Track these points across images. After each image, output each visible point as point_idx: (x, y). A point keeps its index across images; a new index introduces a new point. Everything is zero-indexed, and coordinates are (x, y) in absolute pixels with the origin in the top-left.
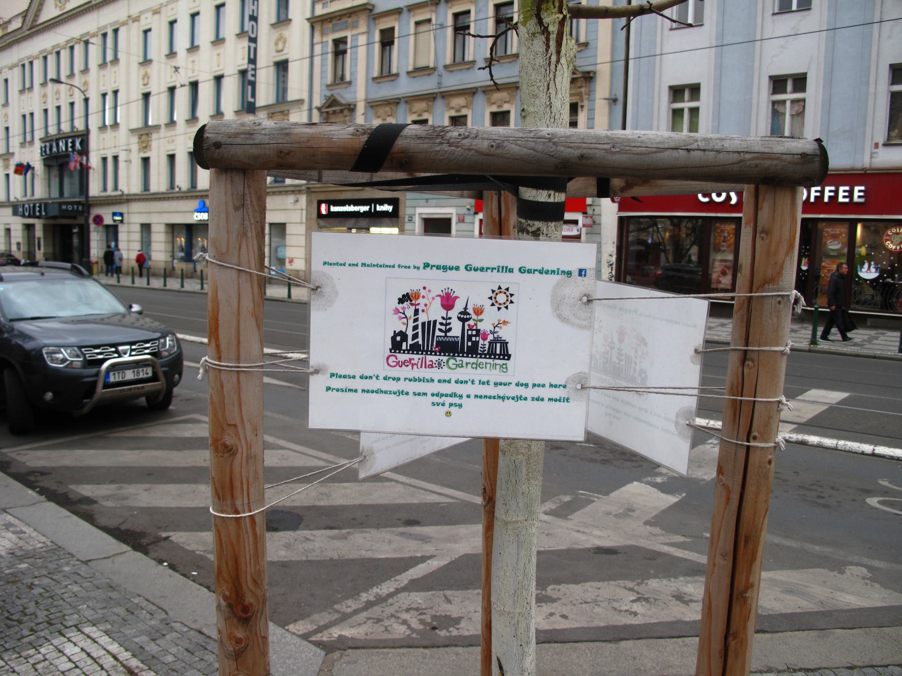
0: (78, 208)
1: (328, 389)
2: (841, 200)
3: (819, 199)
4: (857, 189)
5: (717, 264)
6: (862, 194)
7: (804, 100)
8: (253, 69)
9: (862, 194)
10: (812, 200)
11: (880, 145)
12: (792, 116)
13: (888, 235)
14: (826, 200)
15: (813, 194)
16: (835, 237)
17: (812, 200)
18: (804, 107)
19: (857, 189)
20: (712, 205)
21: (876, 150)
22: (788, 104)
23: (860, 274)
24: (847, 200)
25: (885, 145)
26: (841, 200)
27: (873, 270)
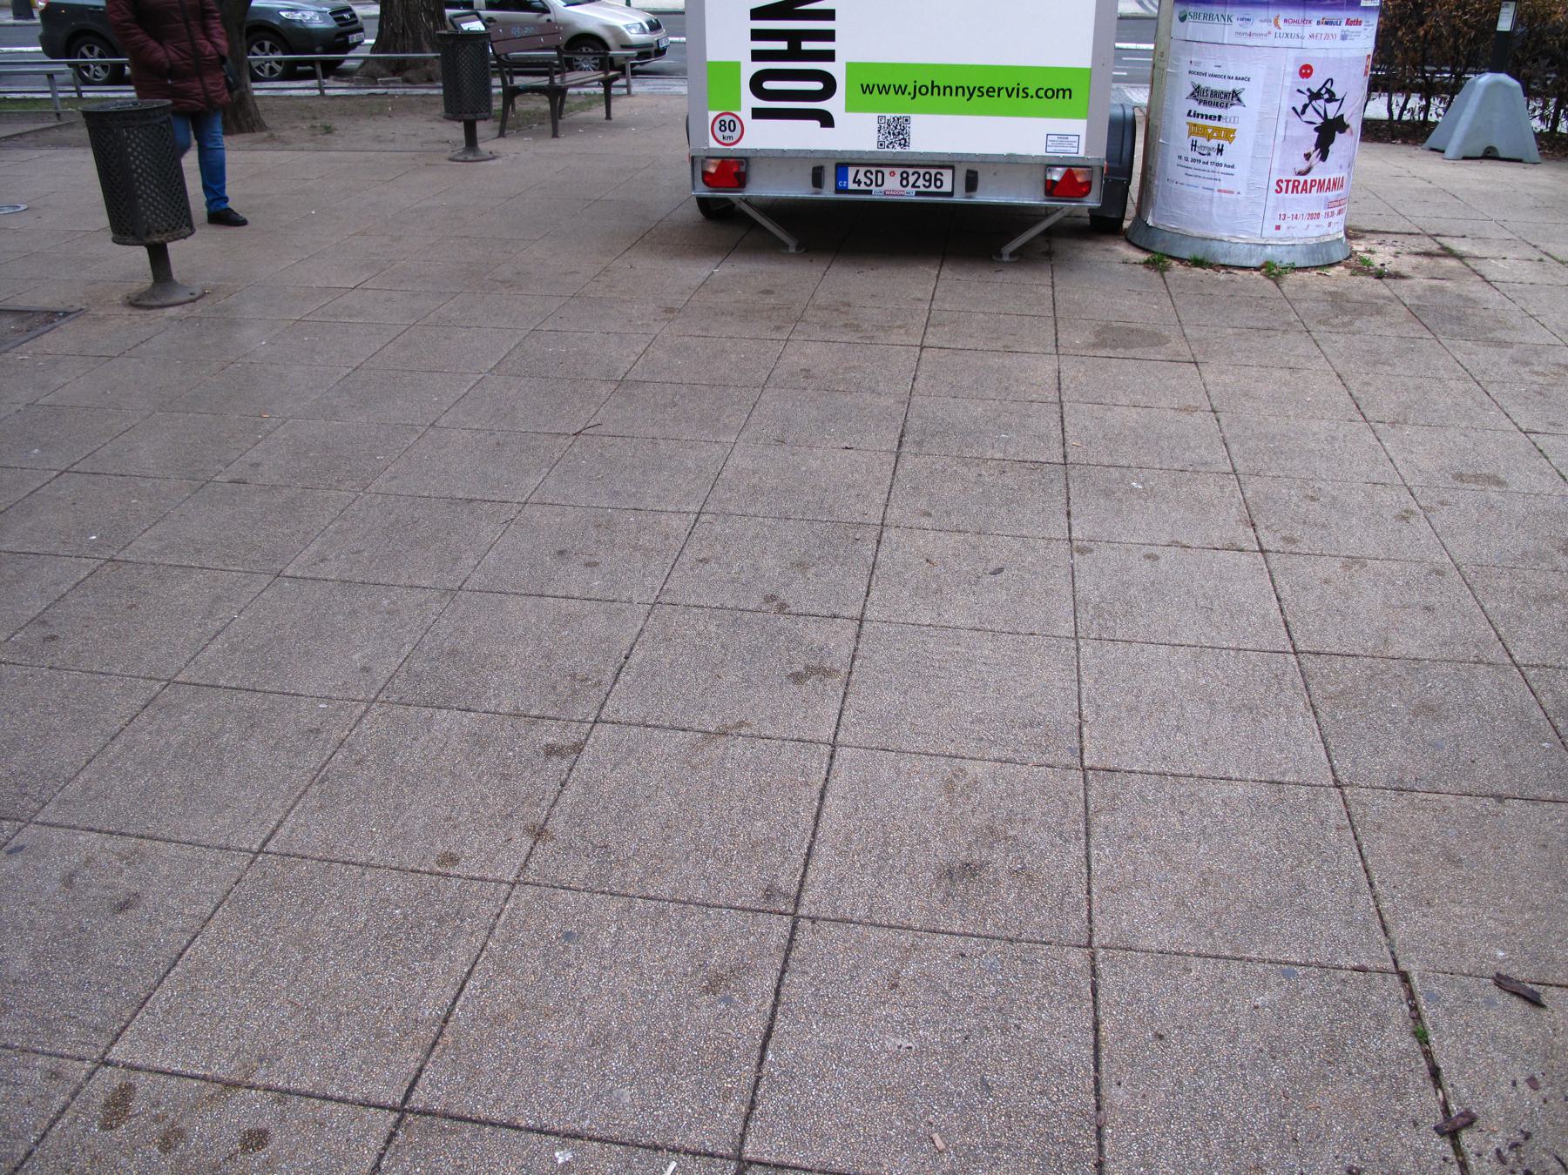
1: (1233, 167)
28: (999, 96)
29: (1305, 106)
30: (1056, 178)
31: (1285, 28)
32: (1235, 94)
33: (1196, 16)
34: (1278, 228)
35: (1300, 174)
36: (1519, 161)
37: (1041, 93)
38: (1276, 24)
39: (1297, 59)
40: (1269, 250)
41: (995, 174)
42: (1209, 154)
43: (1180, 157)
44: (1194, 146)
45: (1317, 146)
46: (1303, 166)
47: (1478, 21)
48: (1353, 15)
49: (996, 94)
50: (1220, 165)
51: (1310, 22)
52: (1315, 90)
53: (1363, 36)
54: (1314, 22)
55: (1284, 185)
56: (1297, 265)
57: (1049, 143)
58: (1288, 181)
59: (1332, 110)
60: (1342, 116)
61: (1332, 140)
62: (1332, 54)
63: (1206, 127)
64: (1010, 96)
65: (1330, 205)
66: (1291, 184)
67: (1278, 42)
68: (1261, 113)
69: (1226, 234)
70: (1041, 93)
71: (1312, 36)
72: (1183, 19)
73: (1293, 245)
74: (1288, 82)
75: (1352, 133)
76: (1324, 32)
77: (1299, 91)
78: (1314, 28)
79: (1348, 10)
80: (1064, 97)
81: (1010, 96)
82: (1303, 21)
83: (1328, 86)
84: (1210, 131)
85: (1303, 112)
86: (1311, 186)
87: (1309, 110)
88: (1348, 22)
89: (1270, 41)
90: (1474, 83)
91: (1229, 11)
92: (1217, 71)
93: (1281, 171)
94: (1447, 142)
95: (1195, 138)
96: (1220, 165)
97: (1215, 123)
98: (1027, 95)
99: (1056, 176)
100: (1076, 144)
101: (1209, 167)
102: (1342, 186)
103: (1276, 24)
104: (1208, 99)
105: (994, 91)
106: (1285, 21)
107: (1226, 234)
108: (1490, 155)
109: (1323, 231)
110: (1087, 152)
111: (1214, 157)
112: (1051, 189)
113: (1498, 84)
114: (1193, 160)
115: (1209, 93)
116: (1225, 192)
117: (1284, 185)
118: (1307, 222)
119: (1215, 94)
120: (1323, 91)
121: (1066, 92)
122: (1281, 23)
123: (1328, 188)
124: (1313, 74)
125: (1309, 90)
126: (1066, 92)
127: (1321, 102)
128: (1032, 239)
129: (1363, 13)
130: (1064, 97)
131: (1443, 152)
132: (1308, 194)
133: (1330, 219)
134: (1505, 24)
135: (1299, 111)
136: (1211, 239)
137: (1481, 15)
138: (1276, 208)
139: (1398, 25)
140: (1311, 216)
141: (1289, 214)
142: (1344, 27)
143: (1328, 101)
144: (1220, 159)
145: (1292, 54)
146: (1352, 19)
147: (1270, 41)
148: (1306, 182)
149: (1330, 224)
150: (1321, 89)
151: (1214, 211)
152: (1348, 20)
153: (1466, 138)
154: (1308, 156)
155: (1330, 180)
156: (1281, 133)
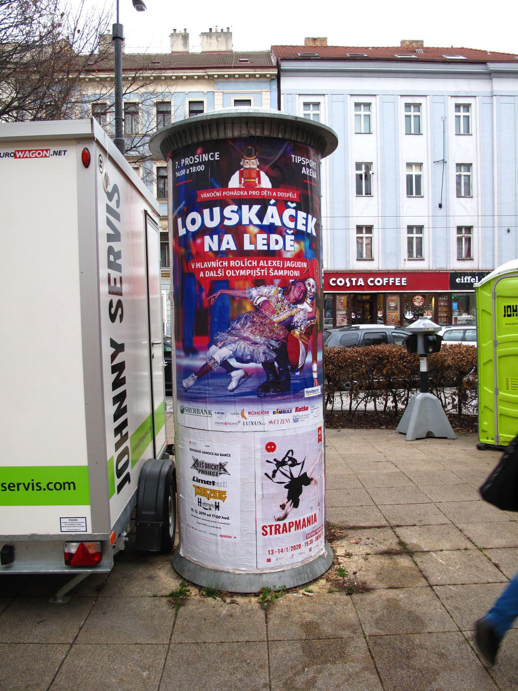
0: (357, 282)
1: (228, 518)
2: (397, 284)
3: (388, 284)
4: (403, 279)
5: (339, 316)
6: (405, 281)
7: (371, 238)
8: (20, 156)
9: (405, 281)
10: (385, 284)
11: (406, 260)
12: (366, 244)
13: (415, 299)
14: (391, 284)
15: (385, 282)
16: (392, 301)
17: (385, 284)
18: (371, 241)
19: (403, 279)
20: (337, 287)
21: (405, 262)
22: (364, 239)
23: (406, 317)
24: (399, 284)
25: (408, 260)
26: (397, 284)
27: (411, 314)
28: (18, 490)
29: (275, 472)
30: (73, 550)
31: (250, 418)
32: (221, 466)
33: (189, 410)
34: (269, 560)
35: (279, 520)
36: (446, 438)
37: (51, 486)
38: (243, 416)
39: (262, 440)
40: (264, 578)
41: (27, 548)
42: (210, 509)
43: (192, 510)
44: (200, 502)
45: (289, 498)
46: (282, 513)
47: (411, 365)
48: (300, 404)
49: (16, 488)
50: (219, 517)
51: (268, 413)
52: (280, 460)
53: (311, 416)
54: (271, 413)
55: (268, 529)
56: (288, 587)
57: (63, 525)
58: (271, 526)
59: (296, 472)
60: (305, 474)
61: (300, 492)
62: (288, 433)
63: (205, 490)
64: (27, 489)
65: (308, 536)
66: (273, 528)
67: (246, 428)
68: (242, 479)
69: (231, 568)
70: (51, 486)
71: (271, 422)
72: (182, 412)
73: (283, 571)
74: (258, 456)
75: (316, 483)
76: (280, 419)
77: (268, 461)
78: (272, 417)
79: (295, 401)
80: (69, 489)
81: (27, 489)
82: (262, 413)
83: (290, 455)
84: (208, 492)
85: (274, 476)
86: (290, 527)
87: (278, 473)
88: (297, 410)
89: (240, 427)
90: (414, 398)
91: (209, 407)
92: (207, 450)
93: (263, 519)
94: (407, 429)
95: (200, 497)
96: (219, 517)
97: (211, 487)
98: (41, 488)
99: (73, 549)
100: (84, 524)
101: (211, 518)
102: (315, 520)
103: (243, 416)
104: (204, 469)
105: (14, 486)
106: (249, 413)
107: (231, 568)
108: (430, 436)
109: (305, 556)
110: (93, 530)
111: (213, 511)
112: (69, 559)
113: (426, 398)
114: (201, 513)
115: (204, 465)
116: (225, 536)
117: (268, 529)
118: (290, 553)
119: (208, 466)
120: (287, 459)
121: (71, 485)
122: (246, 414)
123: (304, 525)
124: (276, 449)
125: (275, 460)
126: (71, 485)
127: (286, 467)
128: (79, 584)
129: (308, 402)
130: (69, 489)
131: (405, 434)
132: (288, 533)
133: (310, 546)
134: (424, 368)
135: (271, 475)
136: (221, 571)
137: (412, 363)
138: (265, 546)
139: (372, 369)
140: (294, 548)
141: (276, 549)
142: (294, 413)
143: (291, 466)
144: (218, 513)
145: (258, 435)
146: (300, 407)
147: (240, 427)
148: (285, 525)
149: (310, 550)
150: (284, 458)
151: (220, 551)
152: (297, 408)
153: (416, 428)
154: (283, 507)
155: (304, 519)
156: (259, 492)
